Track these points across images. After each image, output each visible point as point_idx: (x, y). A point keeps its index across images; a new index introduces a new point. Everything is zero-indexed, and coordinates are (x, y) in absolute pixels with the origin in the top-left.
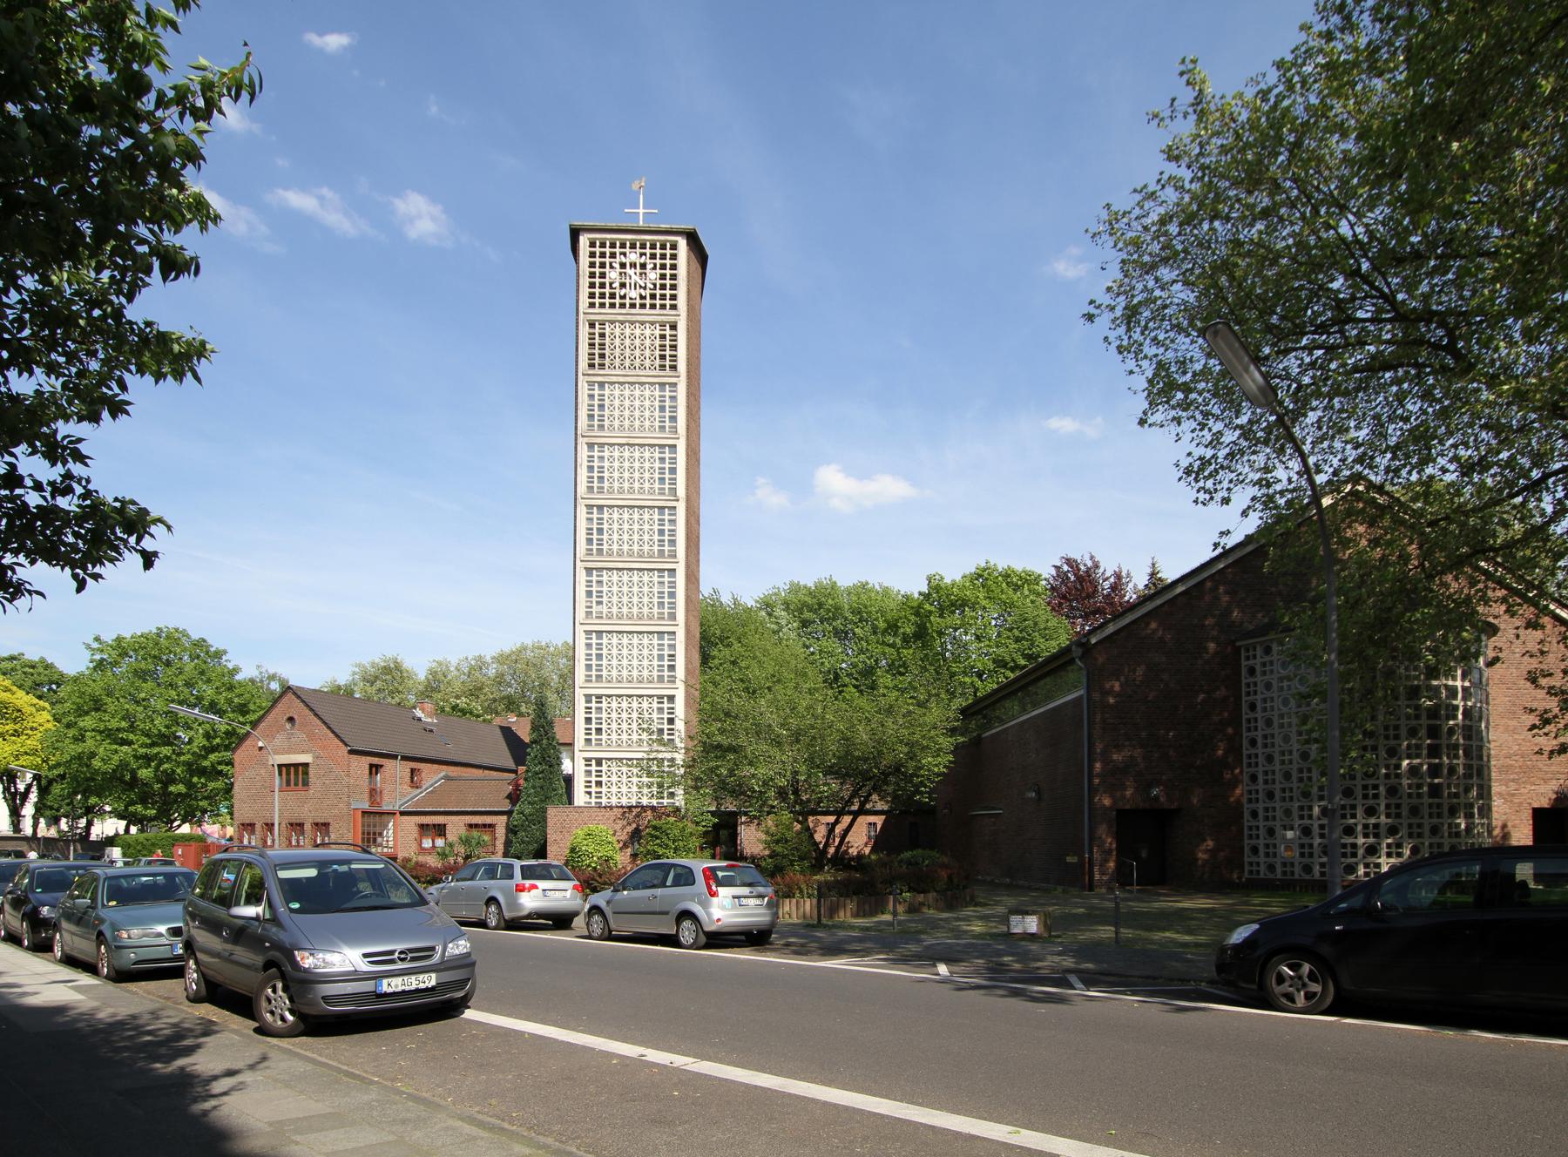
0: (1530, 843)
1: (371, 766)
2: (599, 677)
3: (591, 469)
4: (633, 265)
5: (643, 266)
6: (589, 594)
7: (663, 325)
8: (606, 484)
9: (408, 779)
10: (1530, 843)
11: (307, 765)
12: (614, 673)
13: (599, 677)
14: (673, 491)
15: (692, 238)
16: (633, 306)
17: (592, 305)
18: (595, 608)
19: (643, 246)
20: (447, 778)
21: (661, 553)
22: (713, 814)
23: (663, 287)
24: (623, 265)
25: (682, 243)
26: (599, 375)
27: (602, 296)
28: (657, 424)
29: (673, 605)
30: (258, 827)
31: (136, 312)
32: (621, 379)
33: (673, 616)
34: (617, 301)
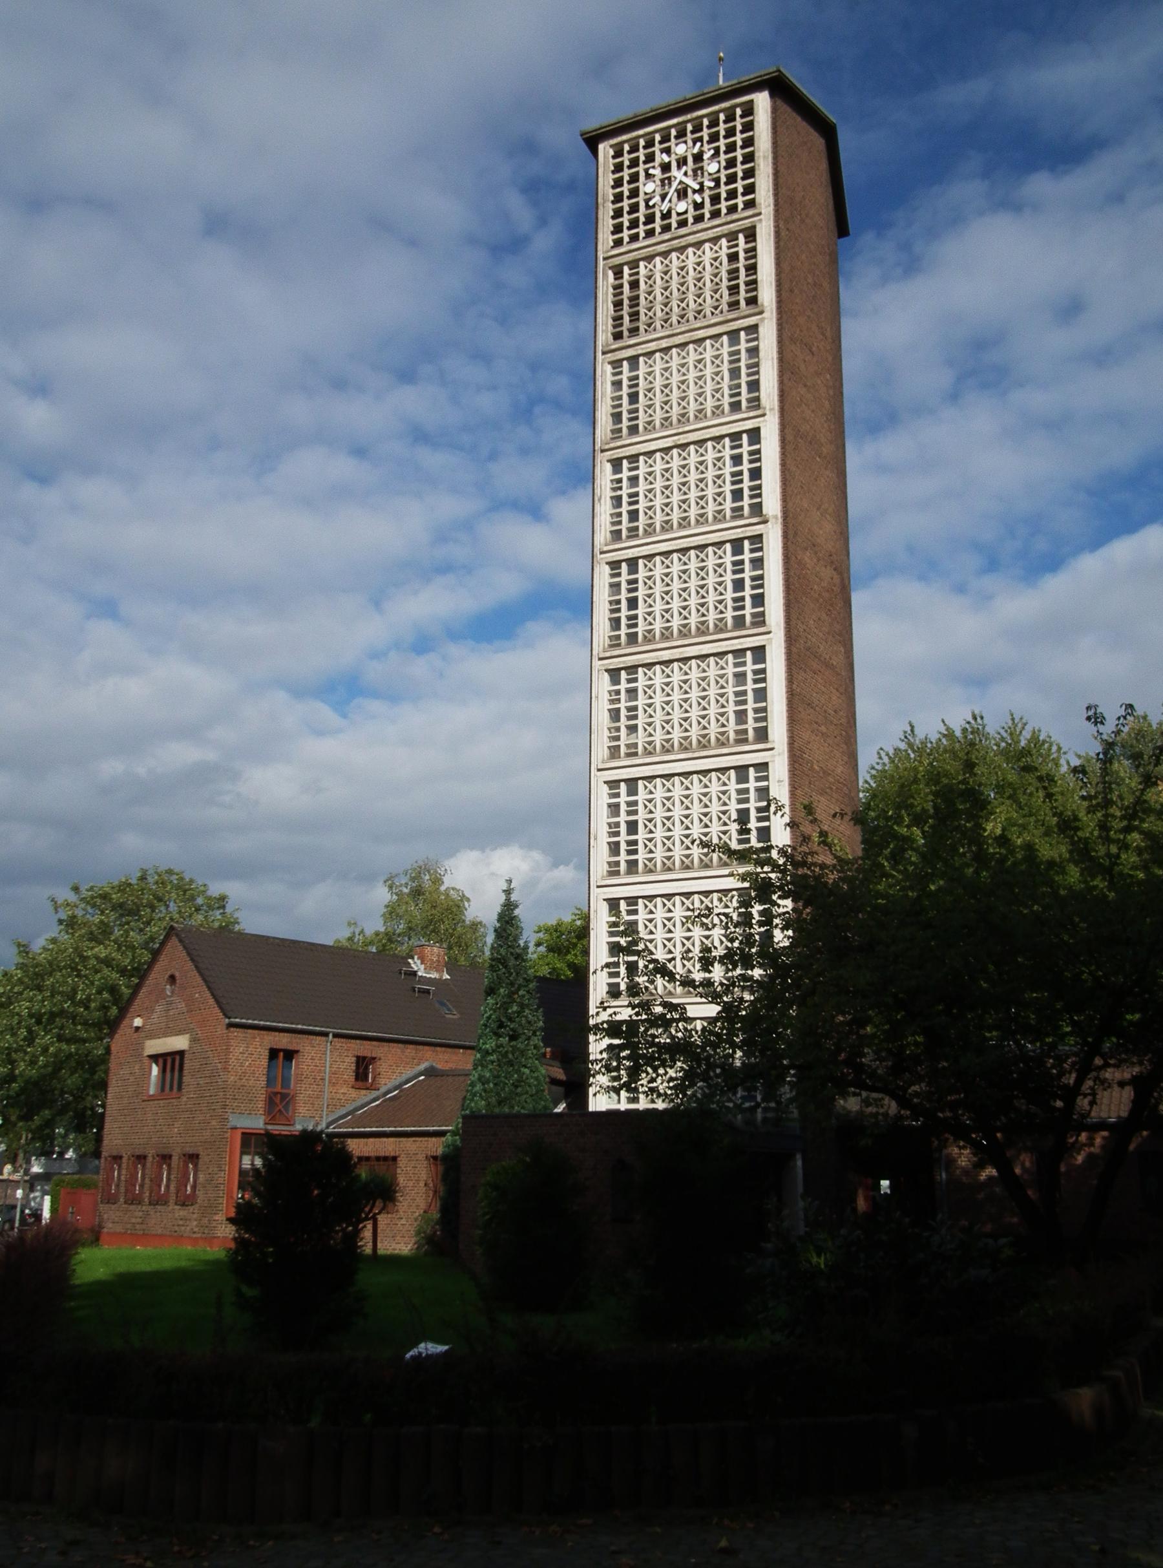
0: (590, 1109)
1: (273, 1053)
2: (632, 866)
3: (617, 501)
4: (682, 162)
5: (698, 158)
6: (615, 715)
7: (732, 237)
8: (642, 520)
9: (349, 1075)
10: (590, 1109)
11: (181, 1053)
12: (659, 854)
13: (632, 866)
14: (757, 509)
15: (779, 87)
16: (683, 224)
17: (618, 243)
18: (624, 739)
19: (698, 128)
20: (430, 1072)
21: (739, 622)
22: (249, 1140)
23: (732, 179)
24: (666, 168)
25: (762, 101)
26: (631, 347)
27: (634, 224)
28: (726, 400)
29: (762, 714)
30: (175, 1159)
31: (835, 862)
32: (664, 344)
33: (762, 735)
34: (658, 224)
